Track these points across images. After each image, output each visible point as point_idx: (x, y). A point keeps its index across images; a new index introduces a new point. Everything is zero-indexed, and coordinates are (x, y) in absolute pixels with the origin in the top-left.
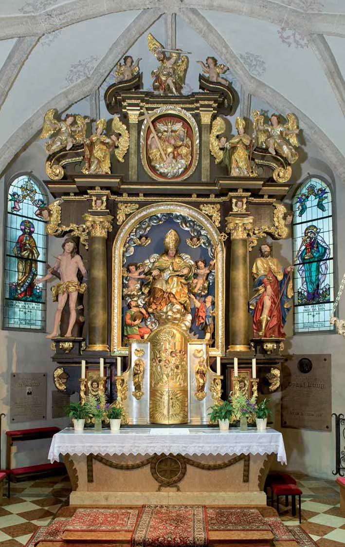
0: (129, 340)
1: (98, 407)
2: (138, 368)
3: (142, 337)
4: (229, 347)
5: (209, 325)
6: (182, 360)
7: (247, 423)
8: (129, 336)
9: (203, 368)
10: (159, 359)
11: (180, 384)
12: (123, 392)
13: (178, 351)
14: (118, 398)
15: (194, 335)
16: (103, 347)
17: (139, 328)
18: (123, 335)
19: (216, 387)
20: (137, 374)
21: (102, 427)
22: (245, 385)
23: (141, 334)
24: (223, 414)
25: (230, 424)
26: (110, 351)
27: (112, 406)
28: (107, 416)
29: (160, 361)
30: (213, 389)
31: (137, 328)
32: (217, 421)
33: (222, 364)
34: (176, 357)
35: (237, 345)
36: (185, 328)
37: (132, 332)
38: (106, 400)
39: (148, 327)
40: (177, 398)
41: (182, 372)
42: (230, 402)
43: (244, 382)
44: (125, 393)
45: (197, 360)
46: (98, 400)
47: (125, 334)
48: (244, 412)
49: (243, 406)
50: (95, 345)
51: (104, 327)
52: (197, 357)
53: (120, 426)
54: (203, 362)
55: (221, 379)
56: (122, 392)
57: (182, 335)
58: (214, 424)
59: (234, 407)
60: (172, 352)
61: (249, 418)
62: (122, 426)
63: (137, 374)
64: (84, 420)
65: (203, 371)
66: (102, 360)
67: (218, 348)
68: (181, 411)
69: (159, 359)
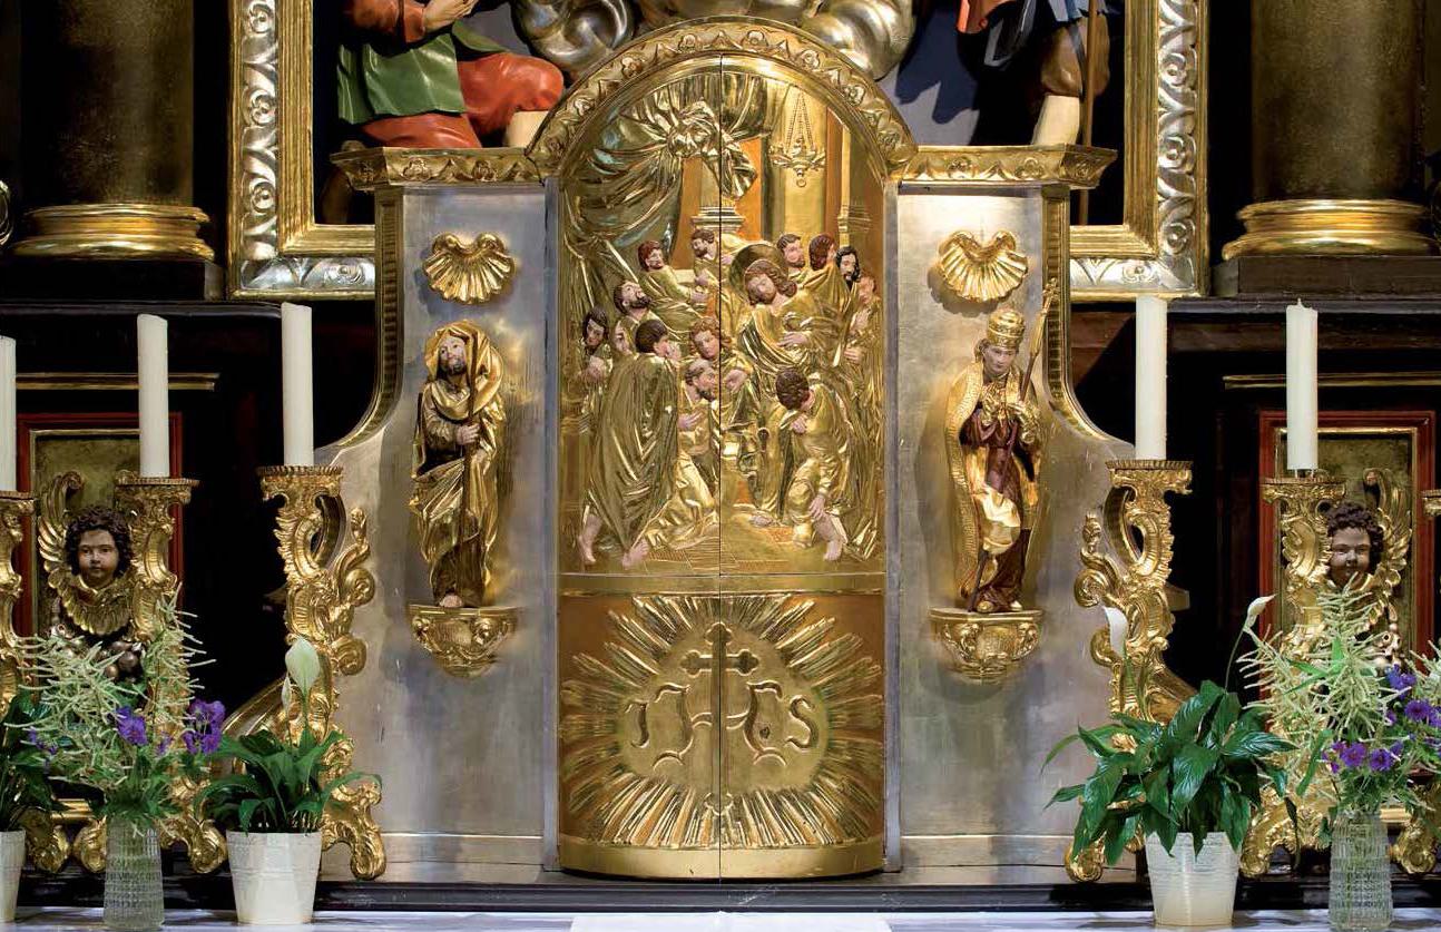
0: (380, 164)
1: (128, 734)
2: (456, 403)
3: (493, 134)
4: (1247, 213)
5: (1071, 23)
6: (835, 327)
7: (1386, 869)
8: (374, 130)
9: (1012, 397)
10: (637, 318)
11: (818, 540)
12: (335, 614)
13: (798, 251)
14: (291, 658)
15: (942, 114)
16: (160, 220)
17: (464, 54)
18: (329, 132)
19: (1128, 562)
20: (460, 451)
21: (170, 904)
22: (1377, 550)
23: (481, 111)
24: (1188, 789)
25: (1242, 881)
26: (221, 258)
27: (243, 724)
28: (208, 810)
29: (646, 339)
30: (1101, 579)
31: (448, 61)
32: (1127, 860)
33: (1177, 363)
34: (782, 301)
35: (1314, 194)
36: (862, 60)
37: (407, 91)
38: (193, 673)
39: (536, 51)
40: (788, 654)
41: (831, 431)
42: (1247, 689)
43: (1368, 524)
44: (349, 619)
45: (964, 336)
46: (130, 673)
47: (348, 111)
48: (1367, 771)
49: (1360, 726)
50: (92, 209)
51: (163, 55)
52: (972, 307)
53: (312, 891)
54: (1014, 347)
55: (1170, 497)
56: (324, 613)
57: (835, 101)
58: (1109, 876)
59: (1283, 736)
60: (746, 257)
61: (1412, 834)
62: (328, 895)
63: (460, 451)
64: (20, 836)
65: (1015, 422)
66: (153, 335)
67: (1145, 229)
68: (823, 768)
69: (637, 318)
